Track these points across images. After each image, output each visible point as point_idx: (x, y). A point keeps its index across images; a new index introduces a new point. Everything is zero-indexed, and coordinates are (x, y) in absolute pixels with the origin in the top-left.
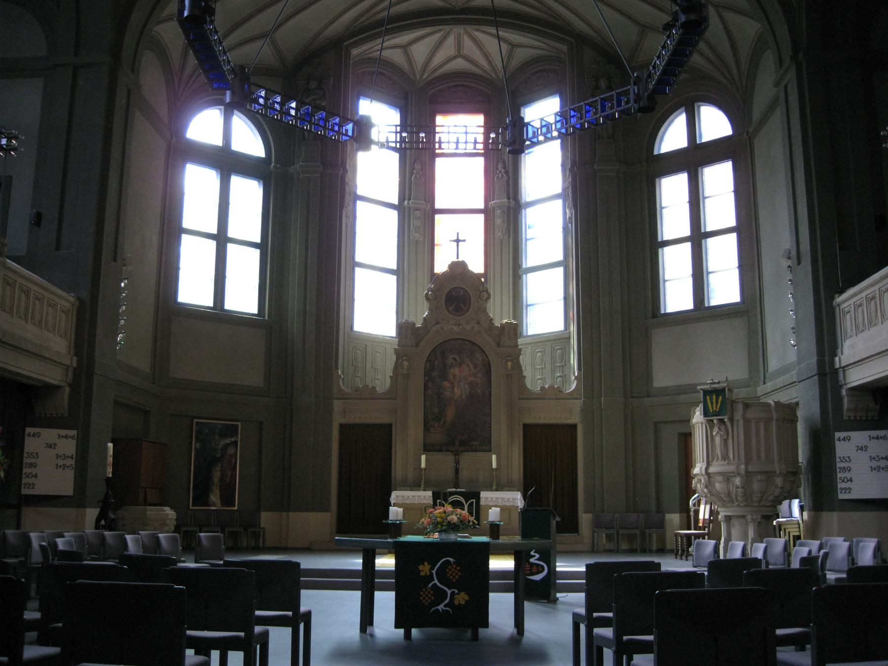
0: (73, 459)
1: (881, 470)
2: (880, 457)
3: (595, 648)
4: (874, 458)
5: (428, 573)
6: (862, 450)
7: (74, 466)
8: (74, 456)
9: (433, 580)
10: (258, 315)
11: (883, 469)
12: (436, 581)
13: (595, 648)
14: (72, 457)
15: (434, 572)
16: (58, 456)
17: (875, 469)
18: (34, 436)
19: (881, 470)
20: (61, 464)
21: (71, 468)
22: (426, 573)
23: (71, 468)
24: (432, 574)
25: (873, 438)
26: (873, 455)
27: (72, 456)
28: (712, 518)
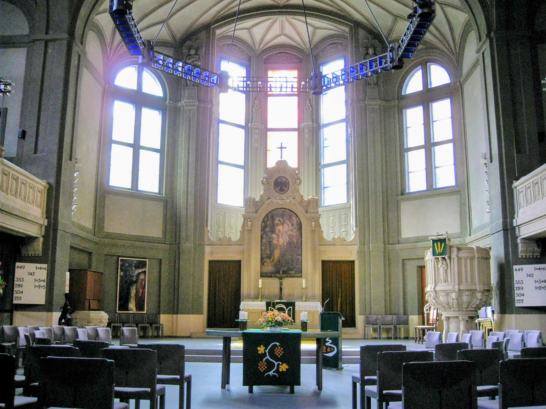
1: (542, 289)
2: (541, 281)
3: (366, 398)
4: (537, 281)
5: (263, 352)
7: (45, 286)
11: (543, 288)
12: (268, 357)
13: (366, 398)
14: (44, 281)
15: (267, 351)
19: (542, 289)
24: (265, 353)
25: (537, 269)
26: (37, 279)
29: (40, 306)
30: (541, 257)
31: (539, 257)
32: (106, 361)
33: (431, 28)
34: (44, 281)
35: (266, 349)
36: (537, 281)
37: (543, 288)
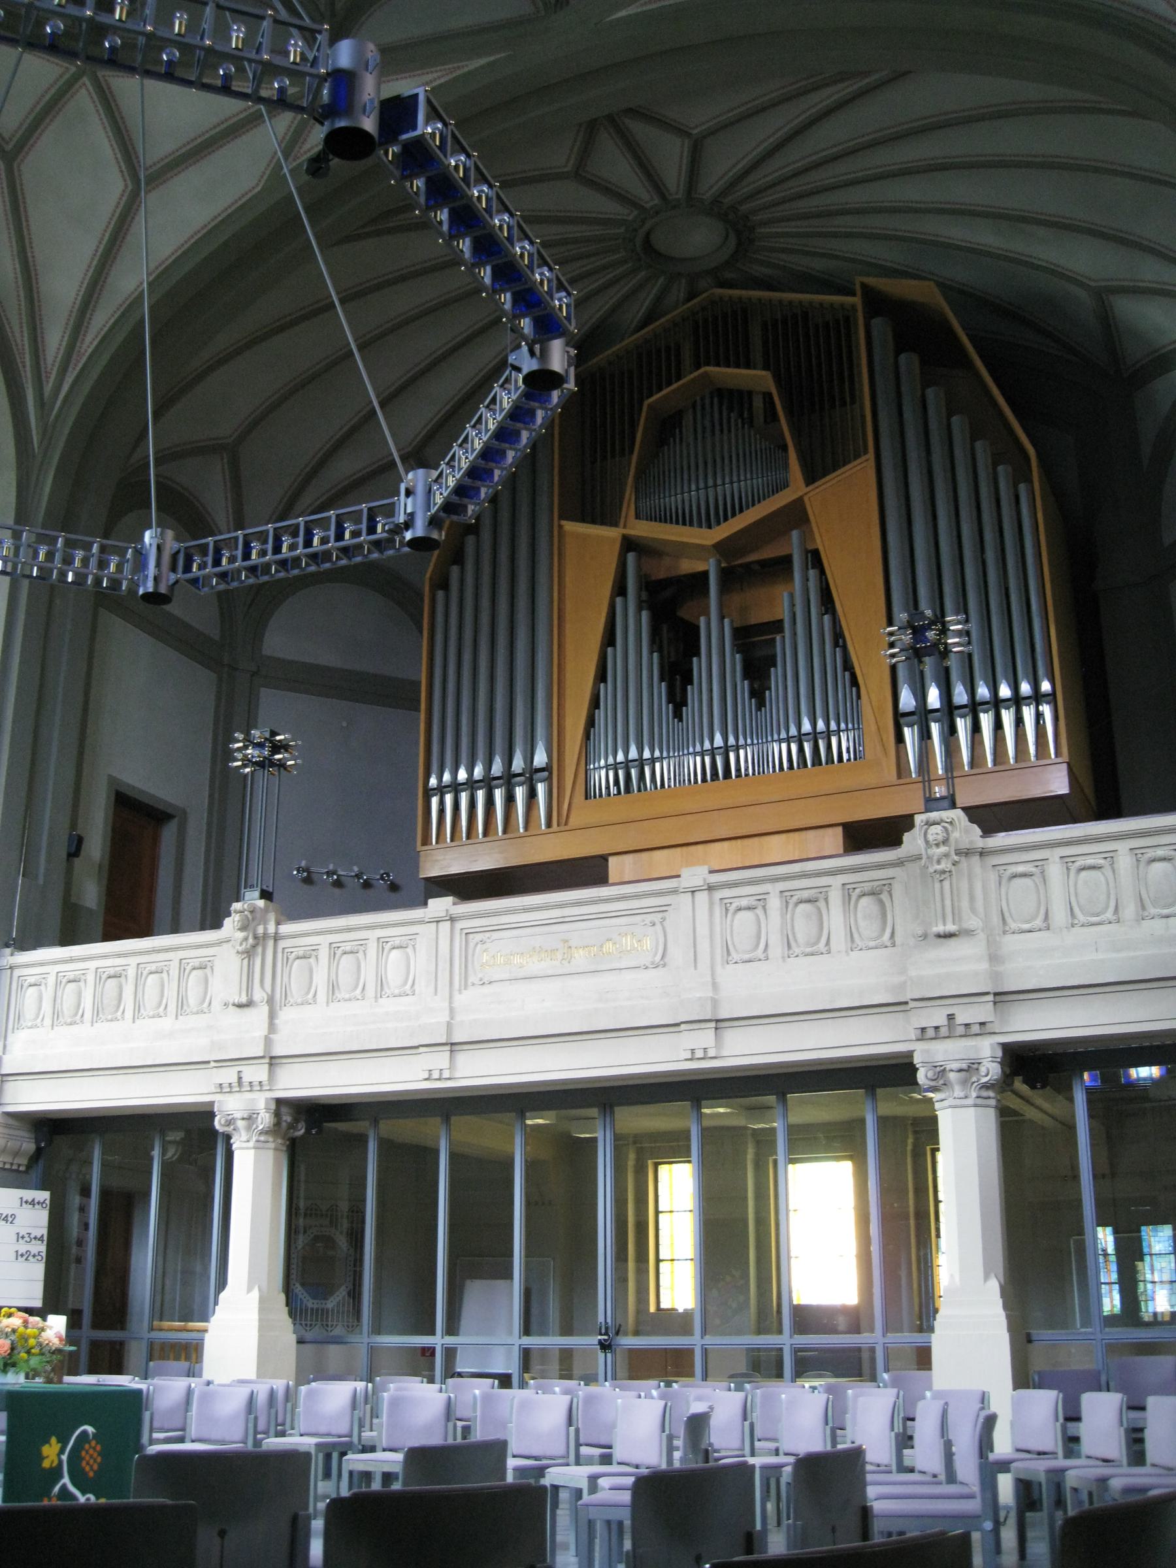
0: (43, 1241)
1: (30, 1258)
2: (32, 1236)
3: (345, 1476)
4: (23, 1237)
5: (56, 1463)
6: (7, 1221)
7: (44, 1254)
8: (45, 1238)
9: (61, 1476)
10: (857, 1156)
11: (34, 1256)
12: (66, 1480)
13: (345, 1476)
14: (41, 1239)
15: (64, 1457)
16: (19, 1237)
17: (22, 1255)
18: (34, 1205)
19: (30, 1258)
20: (24, 1251)
21: (40, 1258)
22: (52, 1462)
23: (40, 1258)
24: (60, 1462)
25: (26, 1202)
26: (23, 1232)
27: (42, 1236)
28: (1146, 1072)
29: (709, 1307)
30: (26, 1172)
31: (21, 1168)
32: (108, 1498)
33: (869, 1468)
34: (41, 1239)
35: (62, 1451)
36: (23, 1237)
37: (34, 1256)
